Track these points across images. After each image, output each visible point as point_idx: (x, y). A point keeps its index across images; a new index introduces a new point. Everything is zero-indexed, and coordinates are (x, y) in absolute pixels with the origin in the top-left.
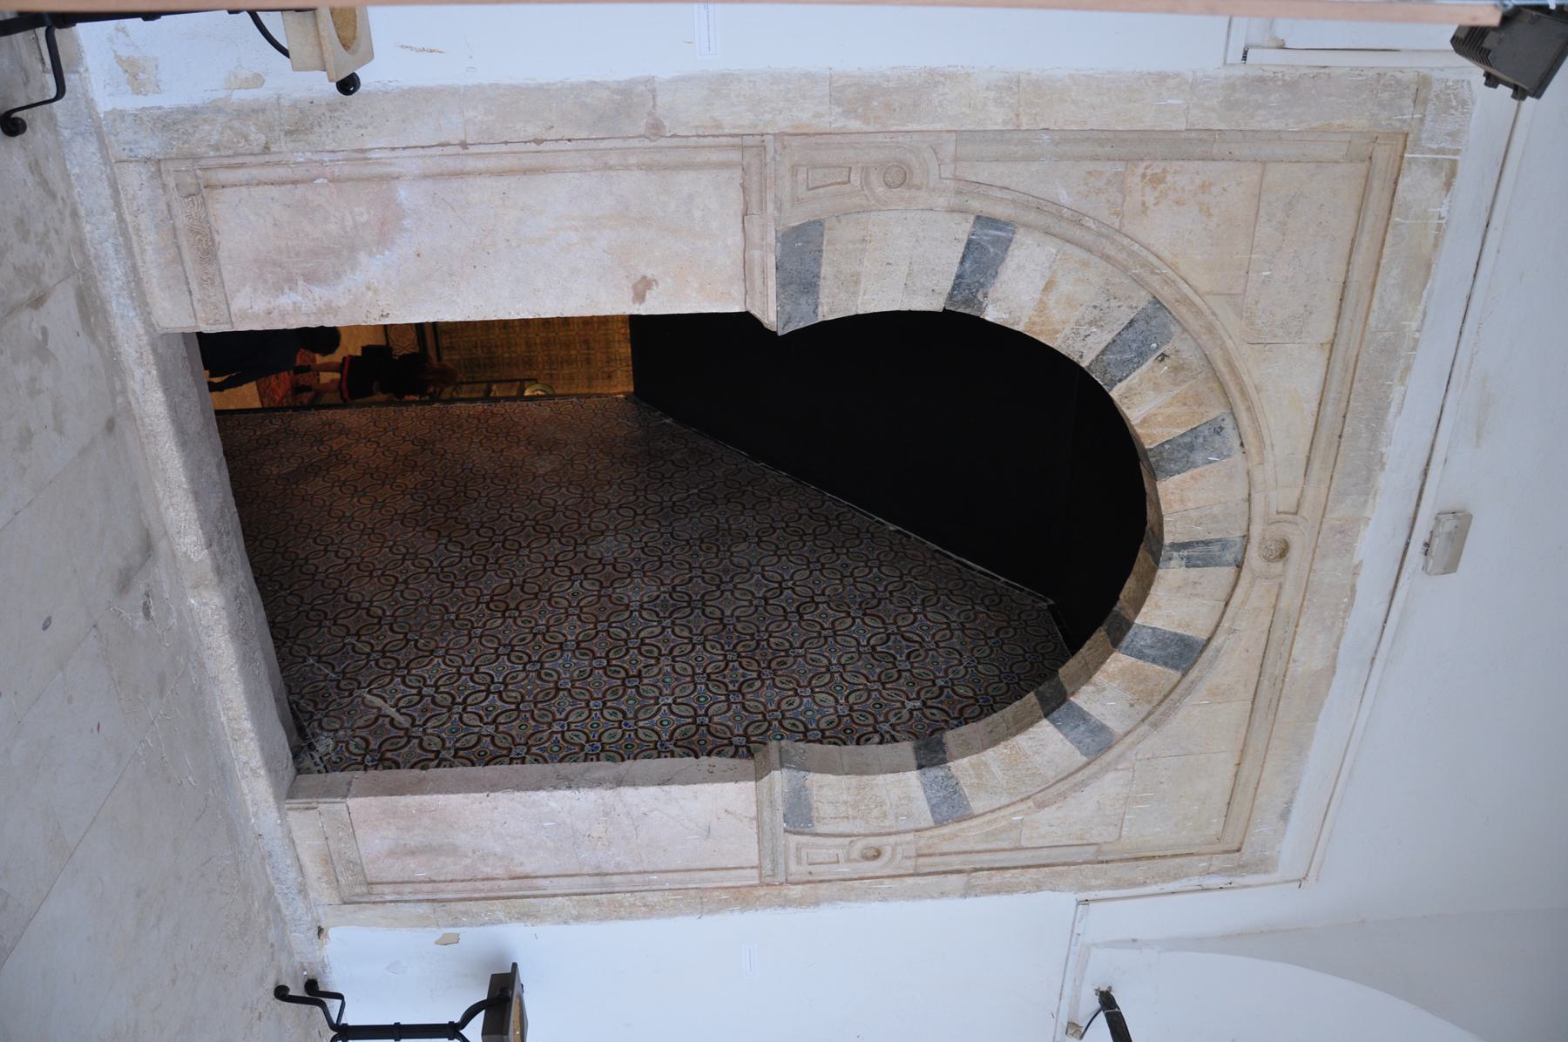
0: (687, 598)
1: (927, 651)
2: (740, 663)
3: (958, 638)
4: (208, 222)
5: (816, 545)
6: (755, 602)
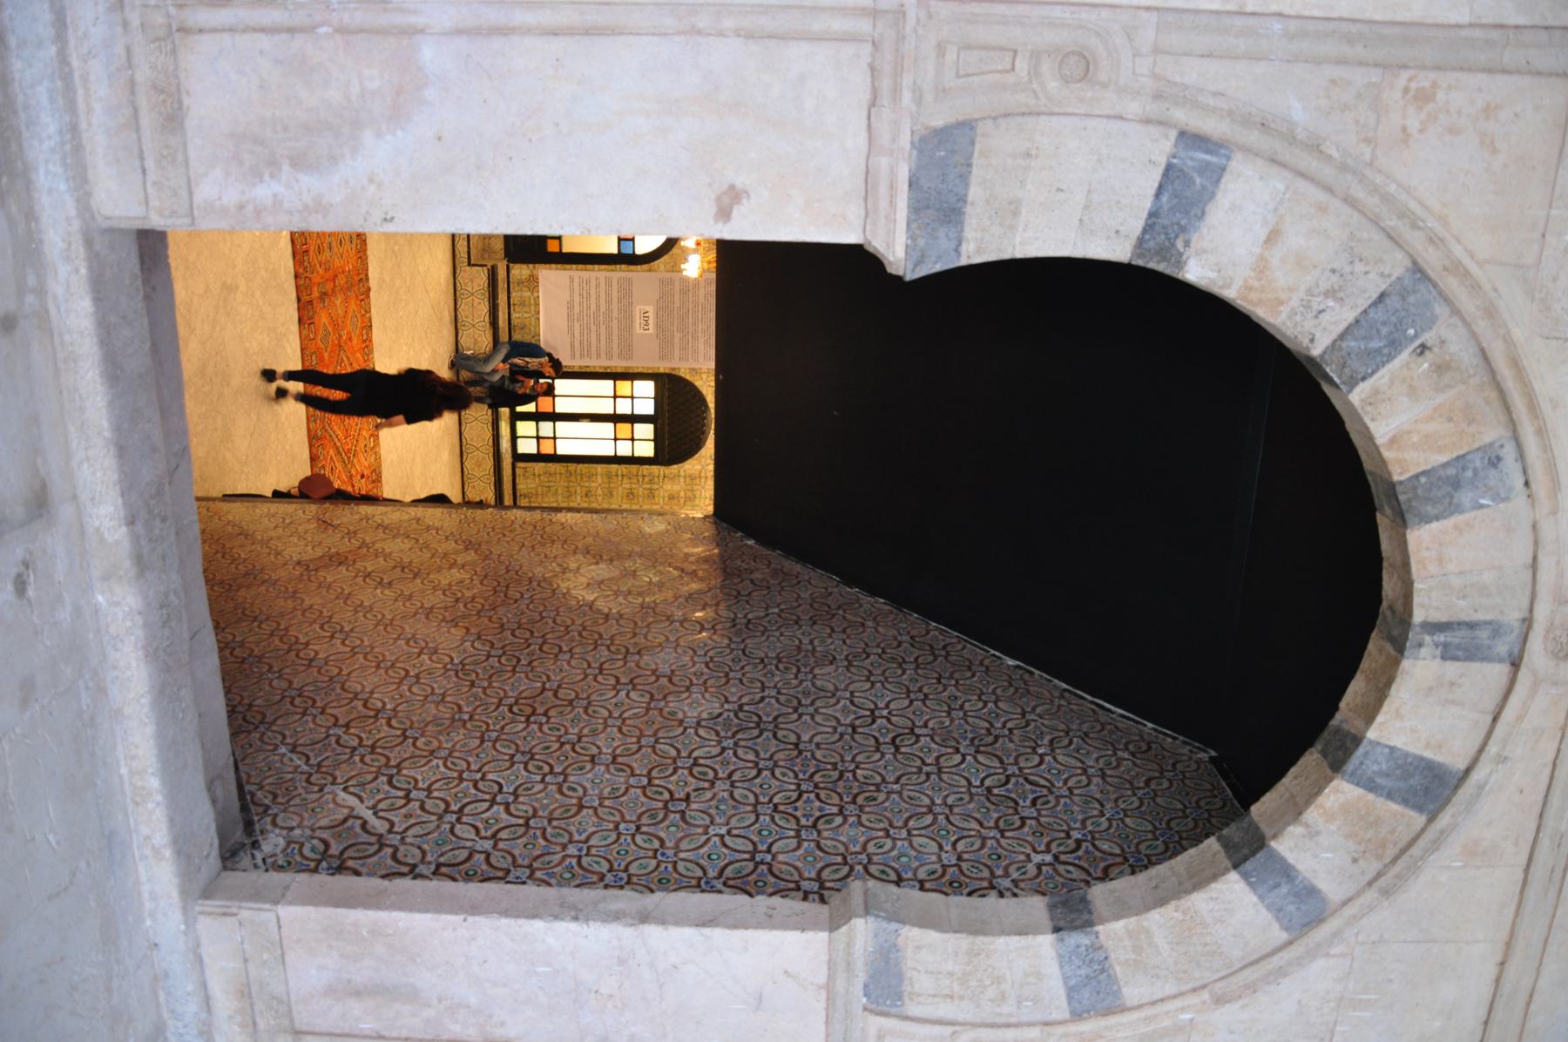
0: (755, 719)
1: (1058, 798)
2: (818, 796)
3: (1098, 785)
4: (177, 77)
5: (918, 675)
6: (840, 729)
